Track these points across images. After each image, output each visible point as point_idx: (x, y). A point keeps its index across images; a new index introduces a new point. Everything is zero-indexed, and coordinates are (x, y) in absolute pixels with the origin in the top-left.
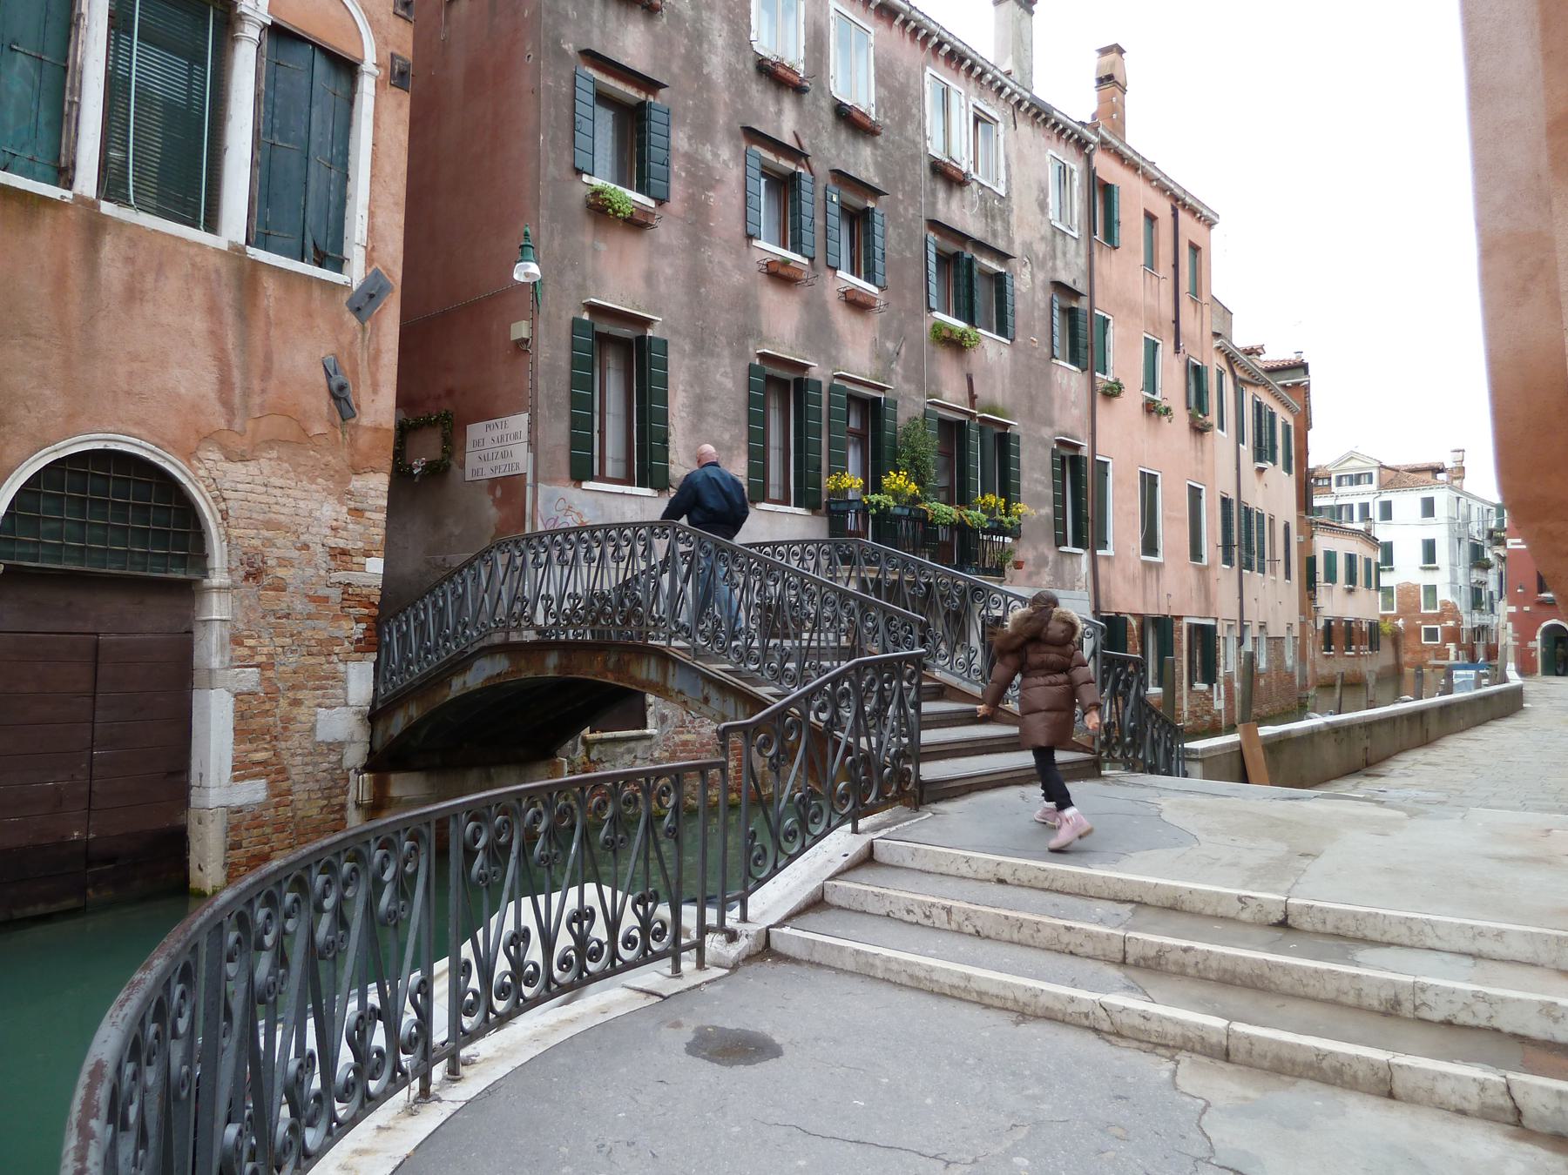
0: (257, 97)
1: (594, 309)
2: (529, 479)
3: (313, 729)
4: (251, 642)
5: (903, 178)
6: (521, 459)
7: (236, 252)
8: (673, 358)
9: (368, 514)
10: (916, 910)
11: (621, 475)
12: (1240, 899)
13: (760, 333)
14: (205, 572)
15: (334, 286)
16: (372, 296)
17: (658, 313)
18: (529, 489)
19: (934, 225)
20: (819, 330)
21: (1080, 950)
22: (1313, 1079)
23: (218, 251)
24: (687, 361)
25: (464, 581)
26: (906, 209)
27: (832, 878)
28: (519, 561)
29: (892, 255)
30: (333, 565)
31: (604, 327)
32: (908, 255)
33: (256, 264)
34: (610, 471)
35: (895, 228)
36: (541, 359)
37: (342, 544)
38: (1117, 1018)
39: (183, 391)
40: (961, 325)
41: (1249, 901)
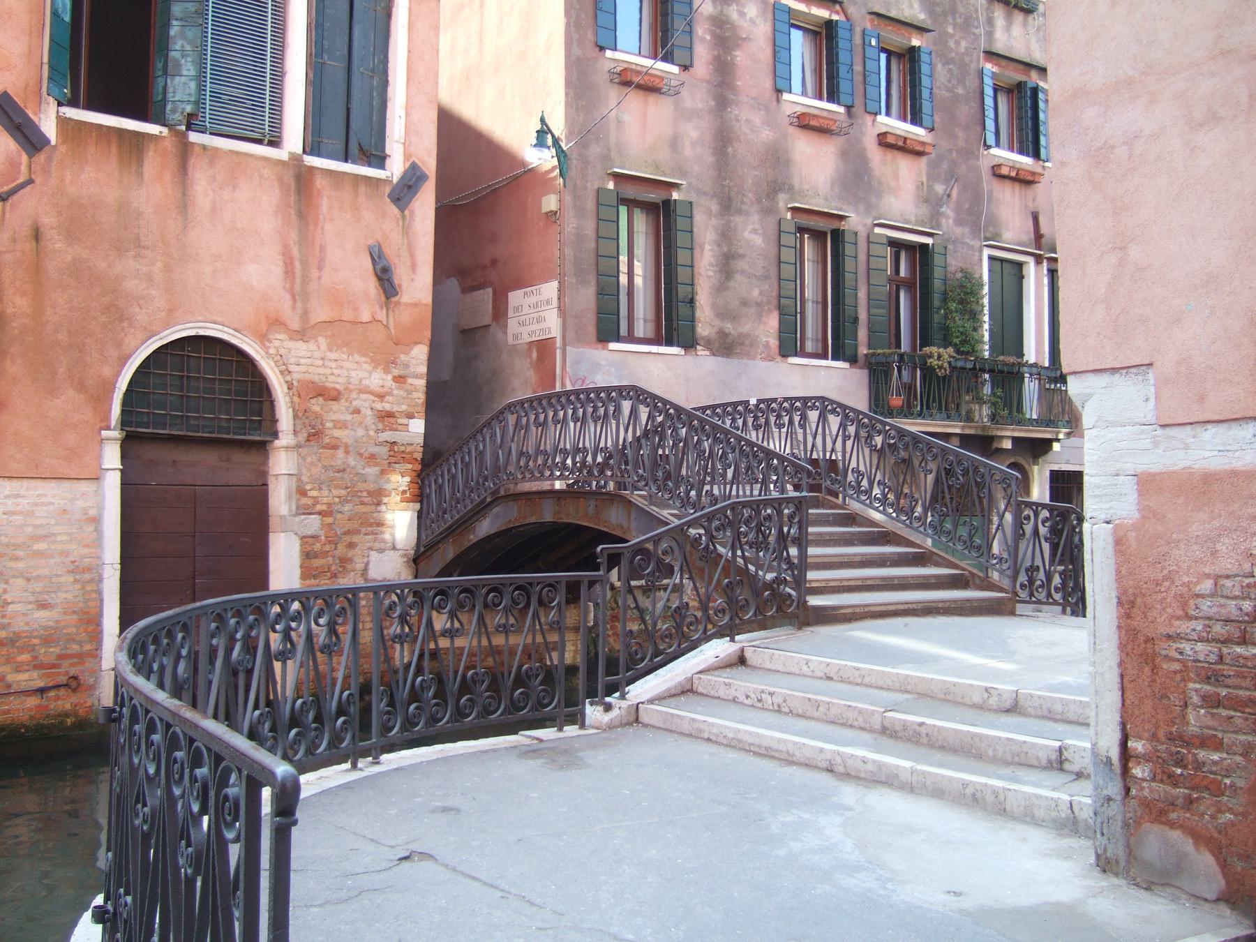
0: (309, 25)
1: (618, 177)
2: (559, 343)
3: (365, 570)
4: (315, 493)
5: (953, 10)
6: (552, 324)
7: (295, 159)
8: (699, 217)
9: (410, 381)
10: (752, 695)
11: (650, 334)
12: (987, 690)
13: (791, 188)
14: (275, 435)
15: (376, 182)
16: (410, 187)
17: (684, 174)
18: (558, 352)
19: (991, 55)
20: (856, 178)
21: (856, 723)
22: (1028, 823)
23: (279, 162)
24: (714, 221)
25: (484, 440)
26: (957, 43)
27: (700, 672)
28: (524, 420)
29: (941, 93)
30: (380, 426)
31: (631, 192)
32: (960, 91)
33: (312, 169)
34: (640, 331)
35: (945, 63)
36: (568, 229)
37: (387, 407)
38: (850, 762)
39: (255, 283)
40: (1026, 161)
41: (993, 692)
